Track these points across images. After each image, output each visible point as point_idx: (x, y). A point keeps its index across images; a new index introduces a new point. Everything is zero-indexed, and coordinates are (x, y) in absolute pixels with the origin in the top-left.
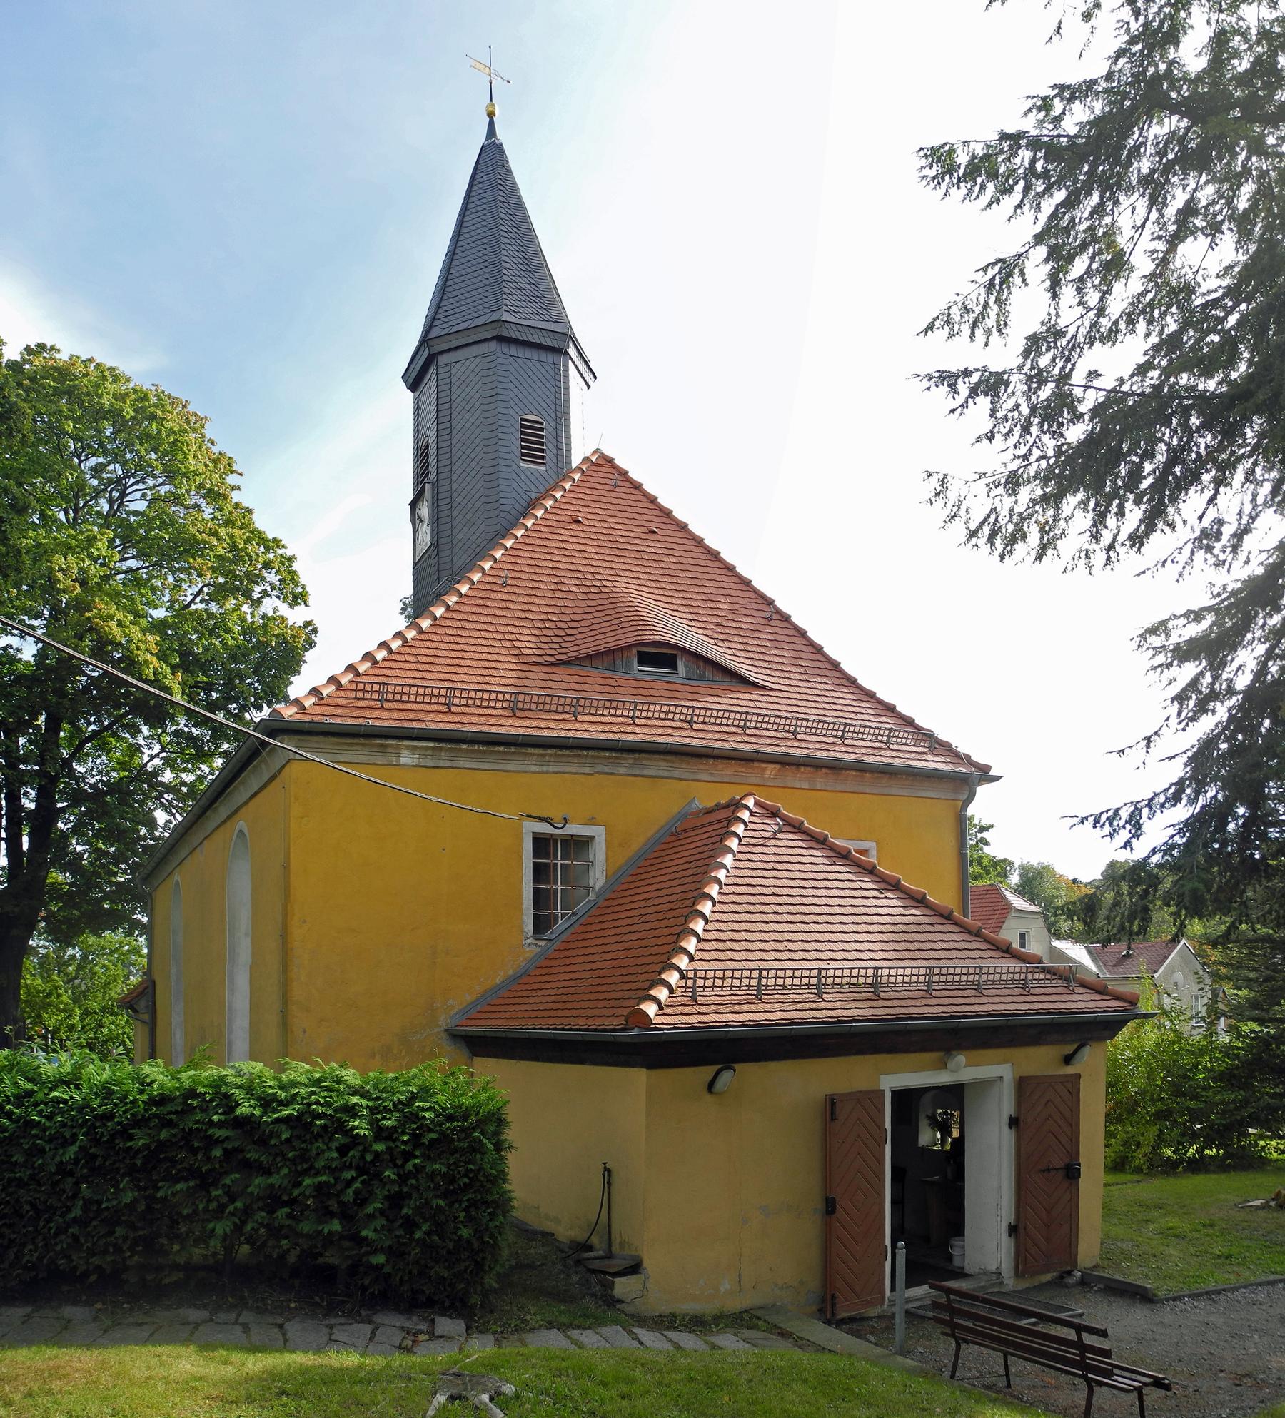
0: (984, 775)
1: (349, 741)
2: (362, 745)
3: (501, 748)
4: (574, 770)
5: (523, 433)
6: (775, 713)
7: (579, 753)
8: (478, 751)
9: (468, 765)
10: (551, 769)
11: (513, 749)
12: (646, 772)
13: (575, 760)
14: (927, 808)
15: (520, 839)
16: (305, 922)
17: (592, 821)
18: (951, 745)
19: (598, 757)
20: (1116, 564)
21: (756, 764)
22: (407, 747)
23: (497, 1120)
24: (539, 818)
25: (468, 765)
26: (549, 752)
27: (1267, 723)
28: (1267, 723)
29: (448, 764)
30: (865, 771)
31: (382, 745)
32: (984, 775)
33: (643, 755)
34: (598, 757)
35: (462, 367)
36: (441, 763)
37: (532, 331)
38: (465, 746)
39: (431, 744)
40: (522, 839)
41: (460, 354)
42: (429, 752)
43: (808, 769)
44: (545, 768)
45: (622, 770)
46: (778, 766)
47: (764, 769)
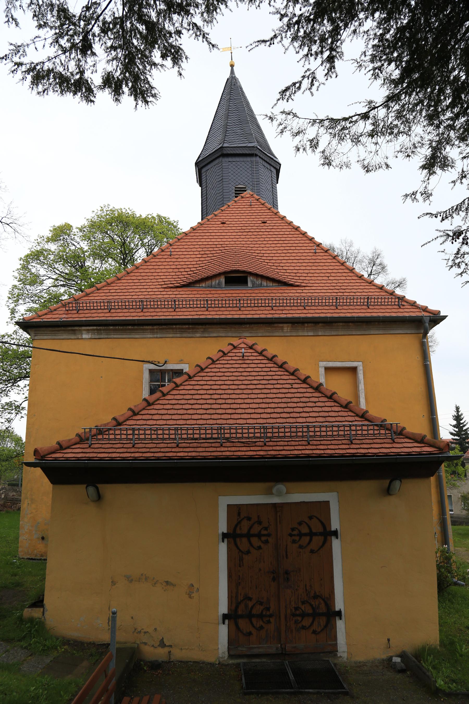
0: (436, 318)
1: (56, 329)
2: (64, 330)
3: (130, 327)
4: (171, 335)
5: (236, 191)
6: (316, 296)
7: (171, 327)
8: (119, 330)
9: (115, 336)
10: (158, 336)
11: (136, 327)
12: (212, 335)
13: (171, 331)
14: (396, 346)
15: (142, 372)
16: (35, 415)
17: (181, 362)
18: (415, 302)
19: (182, 328)
20: (254, 7)
21: (276, 325)
22: (85, 330)
23: (228, 506)
24: (147, 362)
25: (115, 336)
26: (155, 327)
27: (417, 75)
28: (417, 75)
29: (106, 336)
30: (349, 322)
31: (72, 330)
32: (436, 318)
33: (207, 326)
34: (182, 328)
35: (212, 171)
36: (102, 337)
37: (238, 149)
38: (111, 327)
39: (95, 328)
40: (143, 373)
41: (209, 166)
42: (96, 332)
43: (310, 325)
44: (155, 336)
45: (198, 335)
46: (290, 325)
47: (282, 327)
